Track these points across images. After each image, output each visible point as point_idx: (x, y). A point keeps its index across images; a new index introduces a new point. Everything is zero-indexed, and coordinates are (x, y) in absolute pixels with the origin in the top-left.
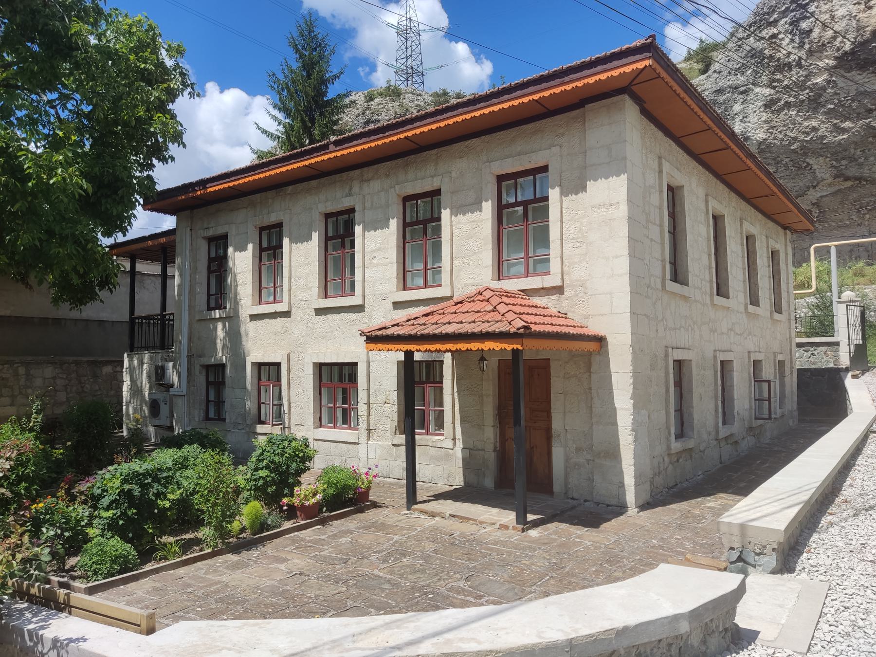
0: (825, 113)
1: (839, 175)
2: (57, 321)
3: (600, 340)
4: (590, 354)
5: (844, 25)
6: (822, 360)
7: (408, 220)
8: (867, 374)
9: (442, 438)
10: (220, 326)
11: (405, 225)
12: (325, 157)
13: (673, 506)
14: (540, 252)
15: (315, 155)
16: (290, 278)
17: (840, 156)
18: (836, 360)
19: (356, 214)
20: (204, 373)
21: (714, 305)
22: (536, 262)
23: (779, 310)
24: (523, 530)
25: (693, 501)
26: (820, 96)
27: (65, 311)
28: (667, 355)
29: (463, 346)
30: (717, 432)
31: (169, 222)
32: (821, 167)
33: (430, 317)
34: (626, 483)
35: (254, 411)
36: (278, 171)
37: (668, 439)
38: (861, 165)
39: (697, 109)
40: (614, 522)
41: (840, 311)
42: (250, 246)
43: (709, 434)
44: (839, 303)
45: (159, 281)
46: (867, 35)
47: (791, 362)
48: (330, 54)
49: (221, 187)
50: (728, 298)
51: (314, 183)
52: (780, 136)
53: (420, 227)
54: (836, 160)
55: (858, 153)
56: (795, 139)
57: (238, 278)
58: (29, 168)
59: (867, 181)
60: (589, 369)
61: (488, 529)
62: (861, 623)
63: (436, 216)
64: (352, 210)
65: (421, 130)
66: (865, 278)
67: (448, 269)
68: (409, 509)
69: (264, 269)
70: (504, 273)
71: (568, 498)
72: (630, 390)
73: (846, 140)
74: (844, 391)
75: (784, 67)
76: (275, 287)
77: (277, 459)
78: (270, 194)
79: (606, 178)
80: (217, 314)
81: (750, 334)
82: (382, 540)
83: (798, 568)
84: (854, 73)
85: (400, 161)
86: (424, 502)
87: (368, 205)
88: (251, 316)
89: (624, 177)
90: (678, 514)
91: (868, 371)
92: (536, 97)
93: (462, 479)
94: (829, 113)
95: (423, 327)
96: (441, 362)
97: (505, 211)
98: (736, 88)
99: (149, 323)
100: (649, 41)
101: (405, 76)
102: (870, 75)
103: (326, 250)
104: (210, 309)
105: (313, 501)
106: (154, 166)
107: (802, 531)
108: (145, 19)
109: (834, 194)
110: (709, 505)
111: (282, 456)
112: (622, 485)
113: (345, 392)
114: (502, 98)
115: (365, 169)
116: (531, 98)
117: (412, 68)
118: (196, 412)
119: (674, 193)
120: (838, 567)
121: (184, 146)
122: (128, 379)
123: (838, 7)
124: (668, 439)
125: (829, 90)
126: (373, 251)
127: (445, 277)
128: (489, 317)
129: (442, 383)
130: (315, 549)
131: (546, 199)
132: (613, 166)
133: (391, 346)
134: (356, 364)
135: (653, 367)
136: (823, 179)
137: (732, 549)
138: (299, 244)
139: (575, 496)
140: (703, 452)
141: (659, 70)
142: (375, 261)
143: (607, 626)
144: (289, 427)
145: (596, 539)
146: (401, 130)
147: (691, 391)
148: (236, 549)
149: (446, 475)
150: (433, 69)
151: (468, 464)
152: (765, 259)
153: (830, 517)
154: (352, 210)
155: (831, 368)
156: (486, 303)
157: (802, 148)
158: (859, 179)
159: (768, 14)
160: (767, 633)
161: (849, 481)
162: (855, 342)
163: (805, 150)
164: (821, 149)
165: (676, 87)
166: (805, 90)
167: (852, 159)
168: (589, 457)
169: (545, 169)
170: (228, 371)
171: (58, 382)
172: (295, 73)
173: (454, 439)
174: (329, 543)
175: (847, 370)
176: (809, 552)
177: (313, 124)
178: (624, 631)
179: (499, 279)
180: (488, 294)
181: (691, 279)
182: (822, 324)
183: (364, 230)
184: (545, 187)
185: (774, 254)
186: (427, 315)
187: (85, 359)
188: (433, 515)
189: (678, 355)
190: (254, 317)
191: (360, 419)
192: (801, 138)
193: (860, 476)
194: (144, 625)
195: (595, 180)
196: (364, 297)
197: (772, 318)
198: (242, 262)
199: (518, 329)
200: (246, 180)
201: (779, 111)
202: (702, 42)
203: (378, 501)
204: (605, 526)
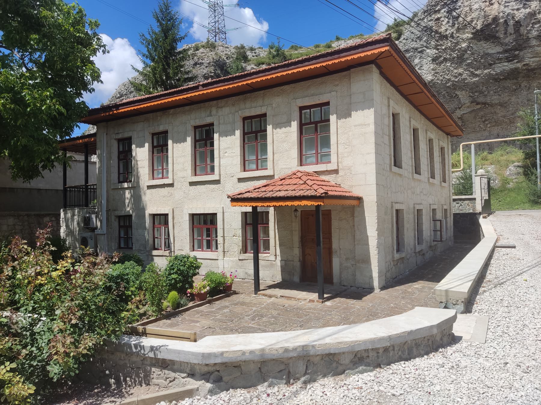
0: (466, 65)
1: (474, 102)
2: (12, 190)
3: (359, 199)
4: (354, 207)
5: (477, 14)
6: (466, 208)
7: (246, 131)
8: (491, 216)
9: (269, 255)
10: (127, 192)
11: (244, 134)
12: (197, 94)
13: (397, 288)
14: (325, 150)
15: (190, 92)
16: (173, 164)
17: (474, 90)
18: (474, 208)
19: (215, 127)
20: (117, 220)
21: (413, 179)
22: (322, 156)
23: (444, 181)
24: (323, 302)
25: (407, 285)
26: (464, 55)
27: (20, 183)
28: (392, 207)
29: (277, 204)
30: (415, 248)
31: (91, 129)
32: (463, 96)
33: (267, 187)
34: (373, 276)
35: (151, 242)
36: (166, 101)
37: (393, 253)
38: (486, 96)
39: (409, 72)
40: (368, 296)
41: (476, 181)
42: (147, 145)
43: (411, 249)
44: (476, 176)
45: (83, 165)
46: (490, 20)
47: (450, 210)
48: (179, 24)
49: (129, 109)
50: (420, 174)
51: (187, 108)
52: (441, 78)
53: (254, 134)
54: (472, 93)
55: (484, 89)
56: (449, 80)
57: (139, 163)
58: (28, 100)
59: (489, 105)
60: (353, 215)
61: (303, 303)
62: (506, 331)
63: (263, 129)
64: (212, 124)
65: (256, 80)
66: (489, 161)
67: (272, 159)
68: (256, 294)
69: (155, 158)
70: (304, 162)
71: (341, 285)
72: (376, 226)
73: (477, 81)
74: (479, 225)
75: (443, 37)
76: (163, 169)
77: (182, 268)
78: (159, 114)
79: (363, 110)
80: (126, 185)
81: (430, 194)
82: (247, 310)
83: (473, 311)
84: (482, 42)
85: (241, 97)
86: (264, 290)
87: (221, 121)
88: (148, 186)
89: (372, 110)
90: (401, 292)
91: (491, 214)
92: (324, 64)
93: (281, 277)
94: (469, 65)
95: (265, 193)
96: (268, 213)
97: (304, 127)
98: (416, 49)
99: (80, 191)
100: (388, 36)
101: (214, 34)
102: (491, 44)
103: (195, 147)
104: (120, 182)
105: (205, 290)
106: (82, 94)
107: (471, 295)
108: (77, 6)
109: (470, 112)
110: (415, 286)
111: (184, 266)
112: (371, 277)
113: (208, 230)
114: (305, 64)
115: (220, 101)
116: (321, 64)
117: (219, 29)
118: (113, 244)
119: (395, 117)
120: (492, 310)
121: (102, 82)
122: (64, 224)
123: (473, 3)
124: (393, 253)
125: (469, 52)
126: (226, 149)
127: (269, 164)
128: (303, 187)
129: (268, 224)
130: (212, 316)
131: (328, 120)
132: (366, 103)
133: (246, 204)
134: (216, 214)
135: (386, 213)
136: (465, 104)
137: (441, 302)
138: (178, 144)
139: (345, 284)
140: (408, 259)
141: (393, 52)
142: (226, 155)
143: (403, 330)
144: (174, 252)
145: (362, 305)
146: (244, 79)
147: (403, 226)
148: (168, 316)
149: (271, 276)
150: (232, 30)
151: (284, 269)
152: (438, 152)
153: (483, 289)
154: (212, 124)
155: (471, 213)
156: (299, 179)
157: (453, 85)
158: (485, 104)
159: (435, 6)
160: (465, 337)
161: (489, 272)
162: (484, 198)
163: (455, 86)
164: (464, 86)
165: (400, 61)
166: (455, 51)
167: (481, 92)
168: (353, 263)
169: (328, 104)
170: (133, 218)
171: (17, 227)
172: (157, 34)
173: (276, 255)
174: (218, 313)
175: (480, 214)
176: (477, 304)
177: (169, 67)
178: (411, 333)
179: (301, 165)
180: (299, 175)
181: (404, 165)
182: (465, 187)
183: (220, 136)
184: (328, 114)
185: (442, 149)
186: (265, 186)
187: (33, 213)
188: (270, 296)
189: (398, 207)
190: (149, 187)
191: (219, 246)
192: (452, 80)
193: (494, 269)
194: (192, 338)
195: (356, 111)
196: (220, 175)
197: (441, 185)
198: (141, 154)
199: (322, 194)
200: (145, 105)
201: (442, 62)
202: (395, 20)
203: (237, 291)
204: (364, 298)
